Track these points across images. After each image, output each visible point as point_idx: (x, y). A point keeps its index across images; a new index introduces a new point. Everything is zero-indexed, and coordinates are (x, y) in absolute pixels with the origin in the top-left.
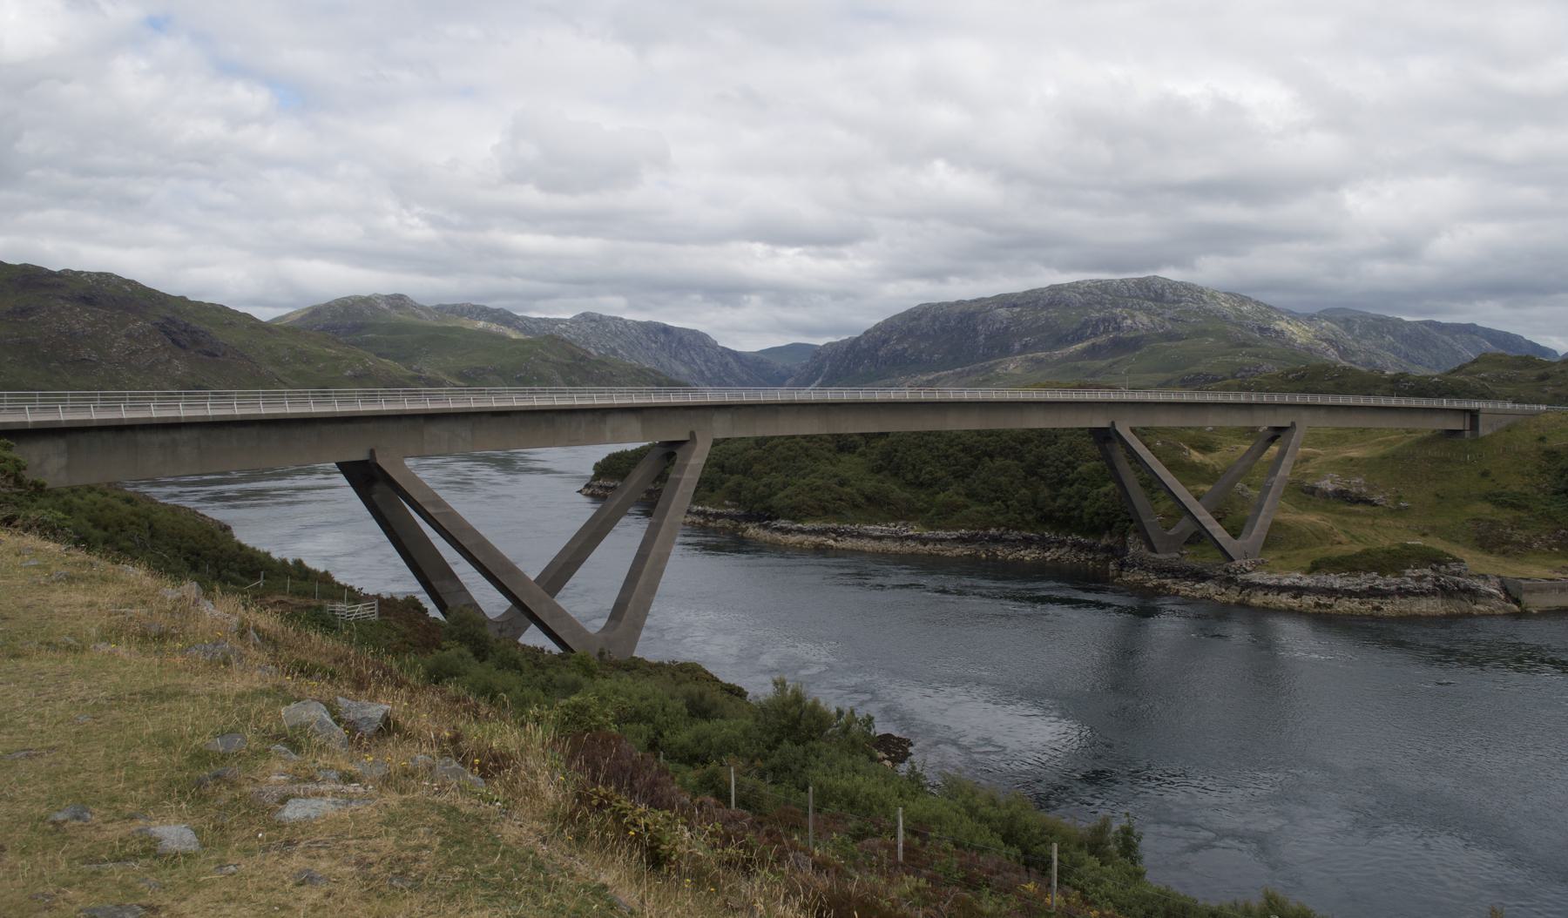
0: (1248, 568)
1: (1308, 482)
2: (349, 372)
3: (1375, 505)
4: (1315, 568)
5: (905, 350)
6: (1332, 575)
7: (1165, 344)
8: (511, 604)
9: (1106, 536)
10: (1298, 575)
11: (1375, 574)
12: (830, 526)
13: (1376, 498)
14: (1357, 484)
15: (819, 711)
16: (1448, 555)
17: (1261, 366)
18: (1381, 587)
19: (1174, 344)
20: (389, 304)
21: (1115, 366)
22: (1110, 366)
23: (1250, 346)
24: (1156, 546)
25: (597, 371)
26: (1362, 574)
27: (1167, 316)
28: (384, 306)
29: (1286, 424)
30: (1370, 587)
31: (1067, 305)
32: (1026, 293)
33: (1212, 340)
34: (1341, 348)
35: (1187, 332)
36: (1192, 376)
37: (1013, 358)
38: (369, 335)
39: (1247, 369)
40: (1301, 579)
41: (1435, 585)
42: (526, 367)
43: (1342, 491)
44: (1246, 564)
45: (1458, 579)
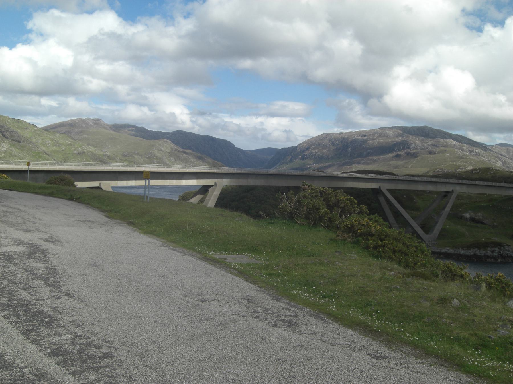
2: (75, 152)
3: (485, 224)
5: (316, 153)
6: (460, 249)
7: (428, 156)
8: (196, 180)
10: (448, 249)
11: (476, 249)
13: (485, 222)
15: (25, 23)
17: (467, 167)
18: (478, 254)
19: (431, 156)
20: (93, 123)
21: (406, 164)
22: (404, 164)
23: (464, 158)
25: (182, 156)
26: (472, 249)
27: (429, 143)
28: (91, 123)
29: (450, 190)
30: (474, 254)
31: (387, 137)
33: (448, 155)
34: (503, 161)
35: (438, 151)
36: (438, 170)
37: (363, 158)
38: (85, 136)
39: (462, 168)
40: (449, 250)
42: (151, 152)
44: (430, 244)
45: (508, 252)
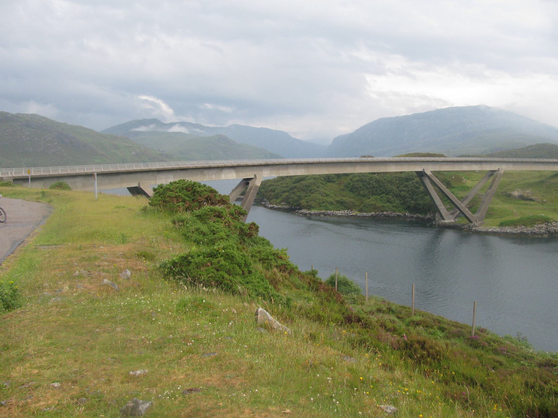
0: (477, 225)
1: (509, 192)
3: (534, 201)
4: (502, 225)
9: (428, 214)
11: (523, 227)
12: (322, 212)
14: (528, 192)
16: (552, 219)
24: (444, 217)
29: (496, 169)
30: (521, 232)
32: (426, 113)
41: (546, 231)
43: (521, 196)
